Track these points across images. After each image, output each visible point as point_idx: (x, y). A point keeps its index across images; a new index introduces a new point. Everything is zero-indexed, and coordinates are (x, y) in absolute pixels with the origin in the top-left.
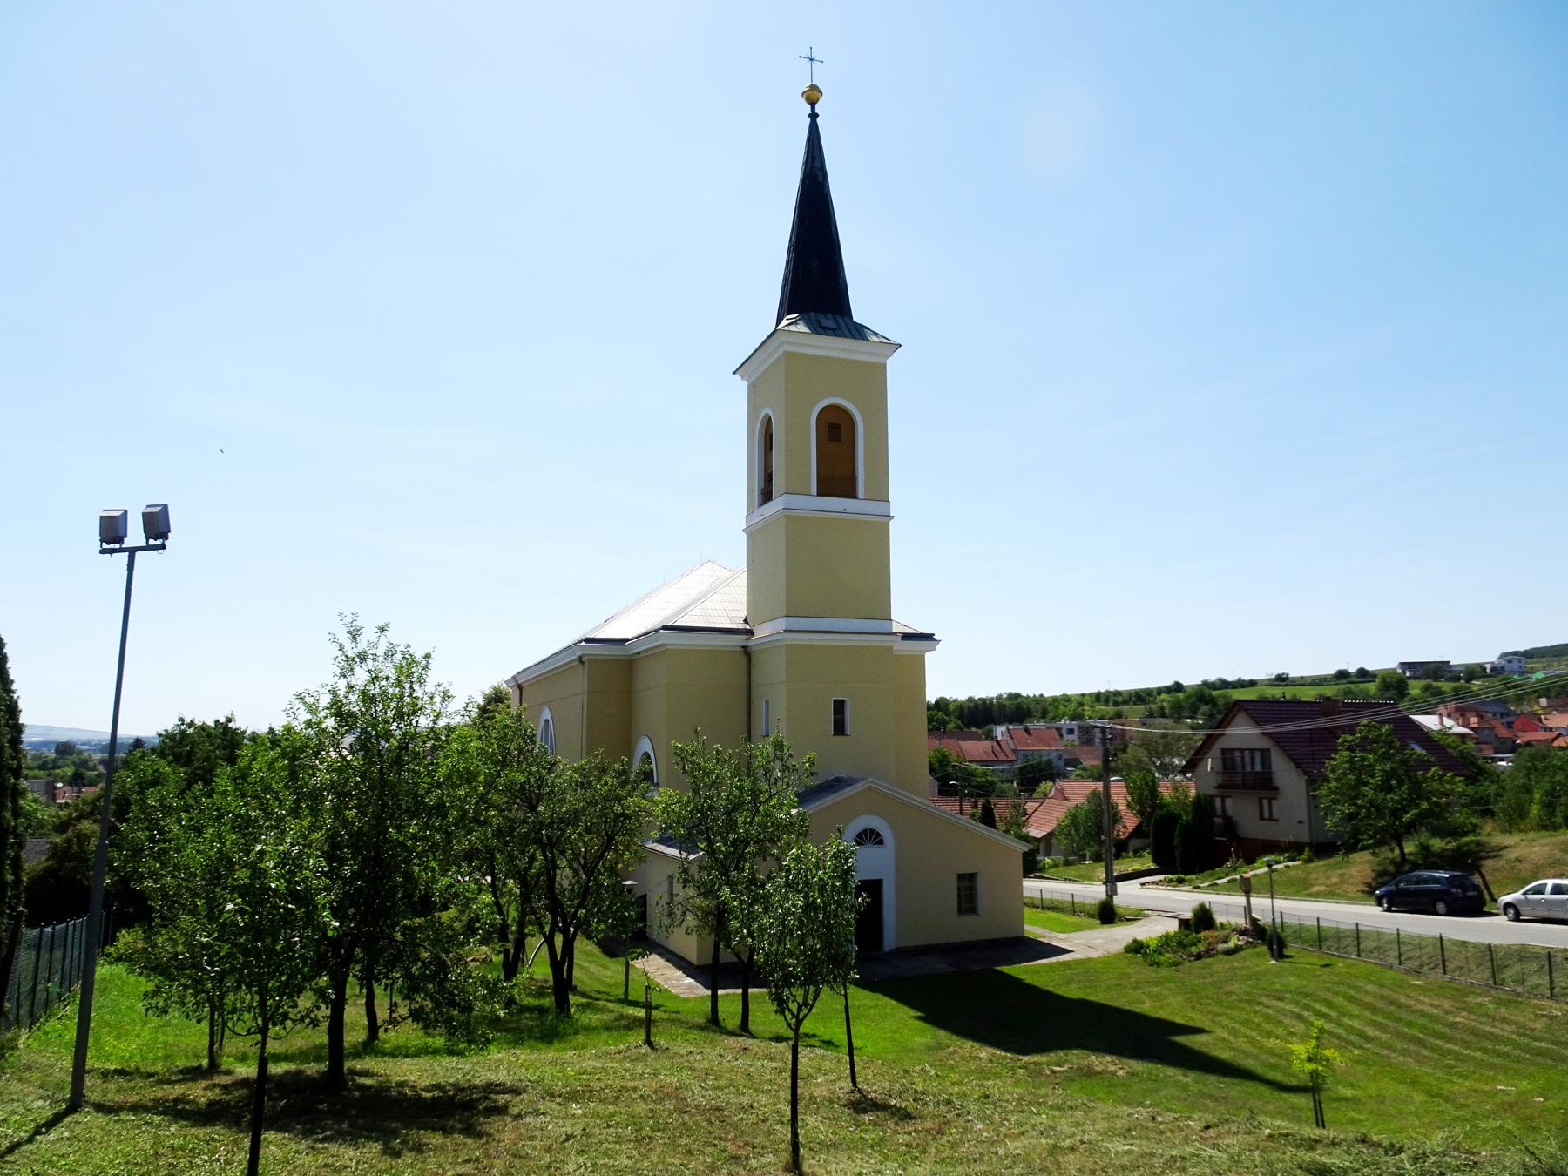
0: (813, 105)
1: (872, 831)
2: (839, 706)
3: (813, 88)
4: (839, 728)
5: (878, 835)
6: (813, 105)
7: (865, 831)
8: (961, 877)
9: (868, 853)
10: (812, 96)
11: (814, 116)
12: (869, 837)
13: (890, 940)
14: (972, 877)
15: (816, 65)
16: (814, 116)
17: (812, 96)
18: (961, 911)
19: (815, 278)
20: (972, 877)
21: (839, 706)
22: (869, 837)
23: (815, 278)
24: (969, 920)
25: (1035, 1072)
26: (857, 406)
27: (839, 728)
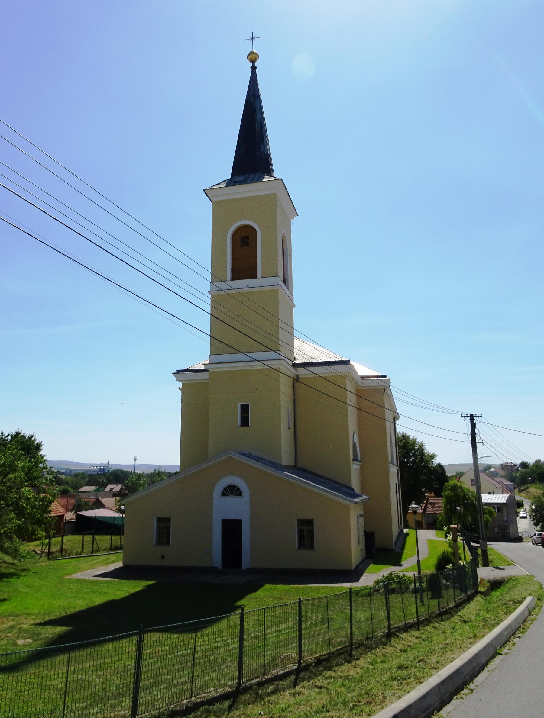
0: (253, 61)
1: (234, 487)
2: (245, 409)
3: (252, 53)
4: (245, 422)
5: (238, 489)
6: (253, 61)
7: (229, 486)
8: (301, 522)
9: (232, 500)
10: (253, 58)
11: (254, 68)
12: (232, 491)
13: (247, 561)
14: (310, 522)
15: (256, 41)
16: (254, 68)
17: (253, 58)
18: (302, 545)
19: (252, 156)
20: (310, 522)
21: (245, 409)
22: (232, 491)
23: (252, 156)
24: (307, 553)
25: (74, 608)
26: (231, 225)
27: (245, 422)
